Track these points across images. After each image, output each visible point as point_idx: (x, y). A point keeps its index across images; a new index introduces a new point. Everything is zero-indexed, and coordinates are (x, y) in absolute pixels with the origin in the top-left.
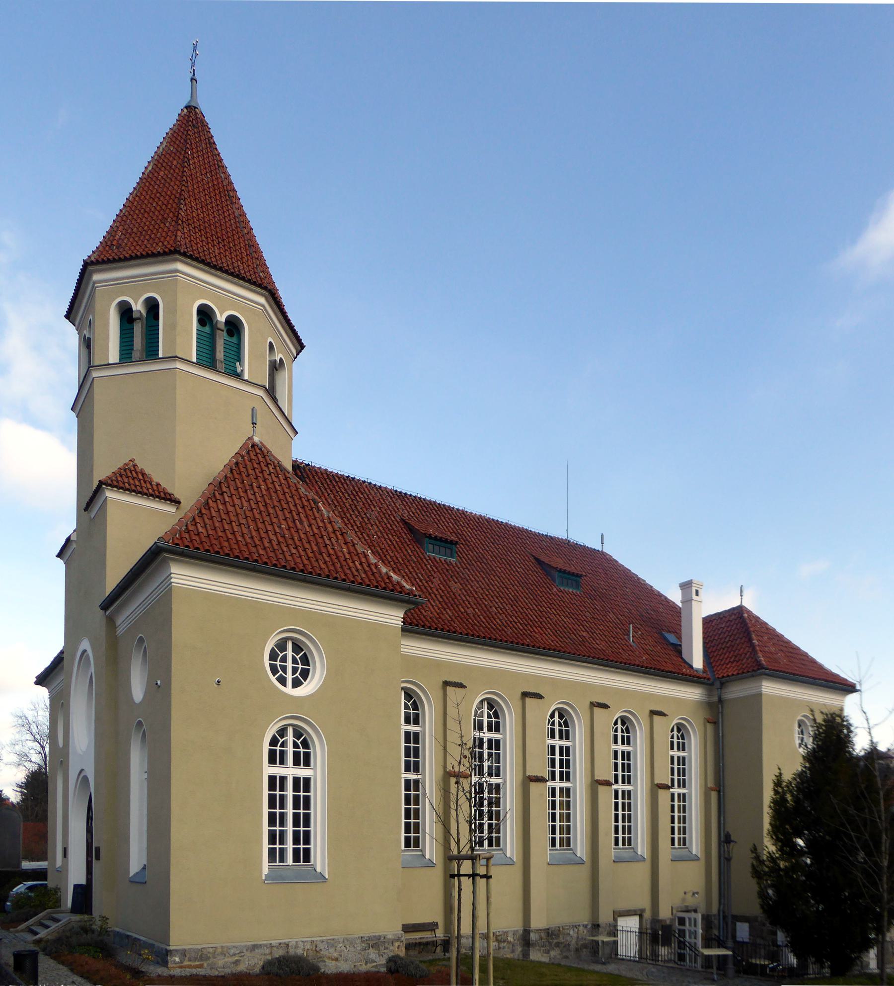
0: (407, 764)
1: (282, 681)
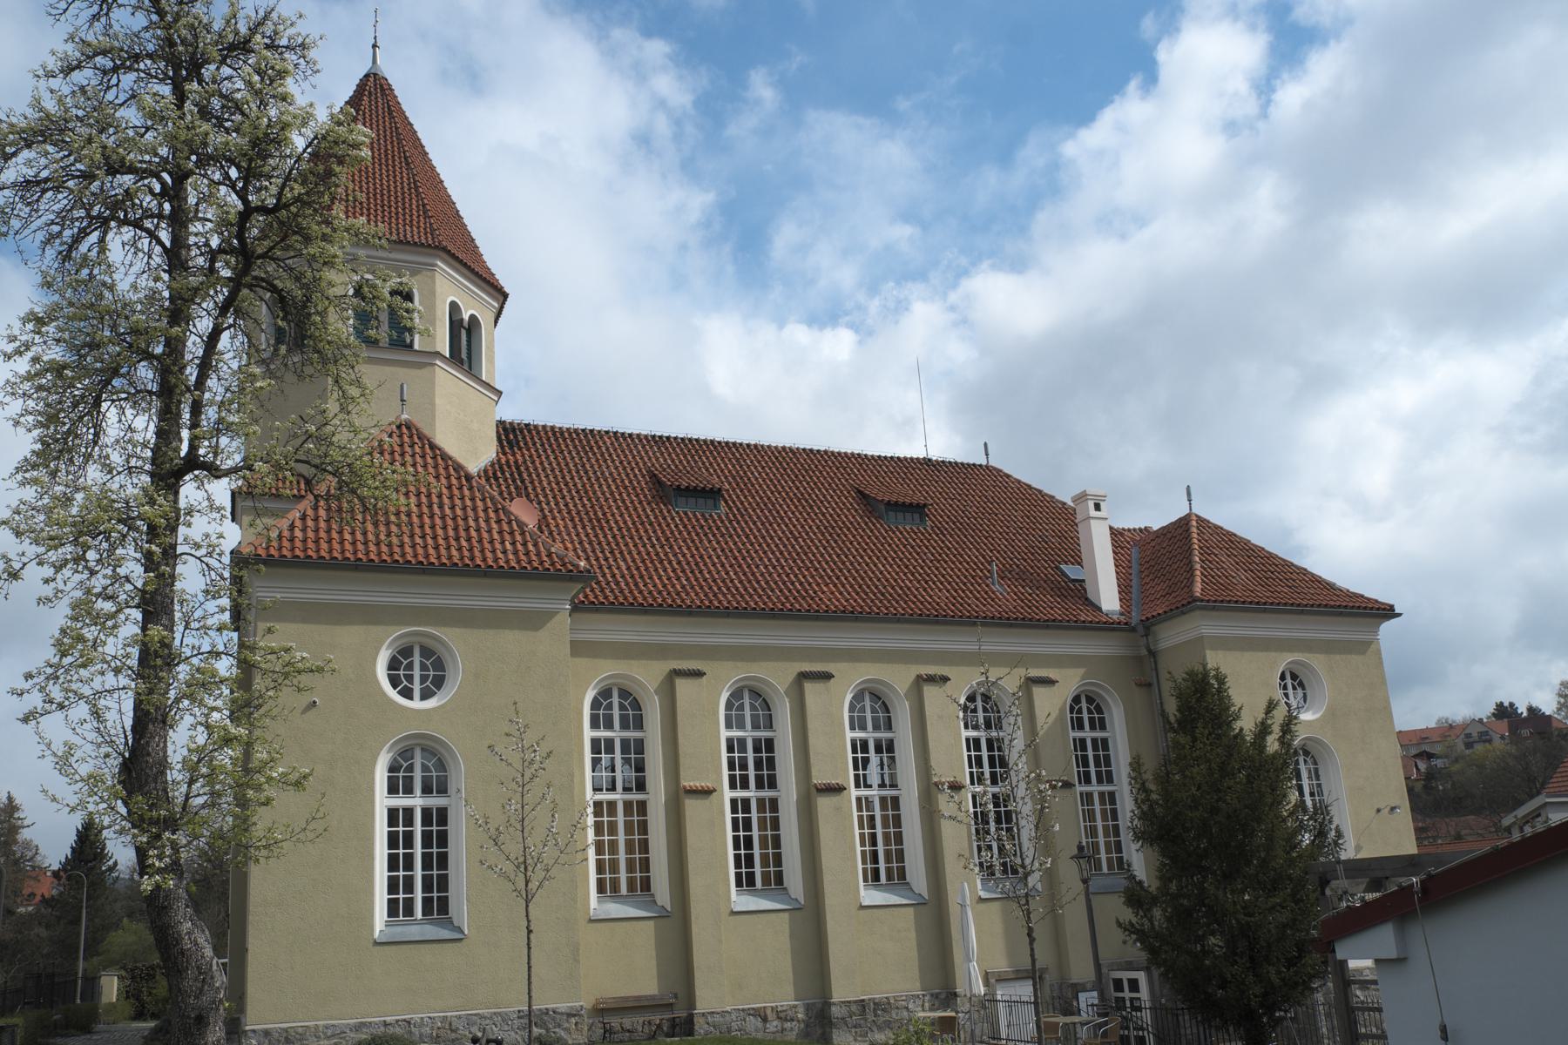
0: (732, 779)
1: (407, 693)
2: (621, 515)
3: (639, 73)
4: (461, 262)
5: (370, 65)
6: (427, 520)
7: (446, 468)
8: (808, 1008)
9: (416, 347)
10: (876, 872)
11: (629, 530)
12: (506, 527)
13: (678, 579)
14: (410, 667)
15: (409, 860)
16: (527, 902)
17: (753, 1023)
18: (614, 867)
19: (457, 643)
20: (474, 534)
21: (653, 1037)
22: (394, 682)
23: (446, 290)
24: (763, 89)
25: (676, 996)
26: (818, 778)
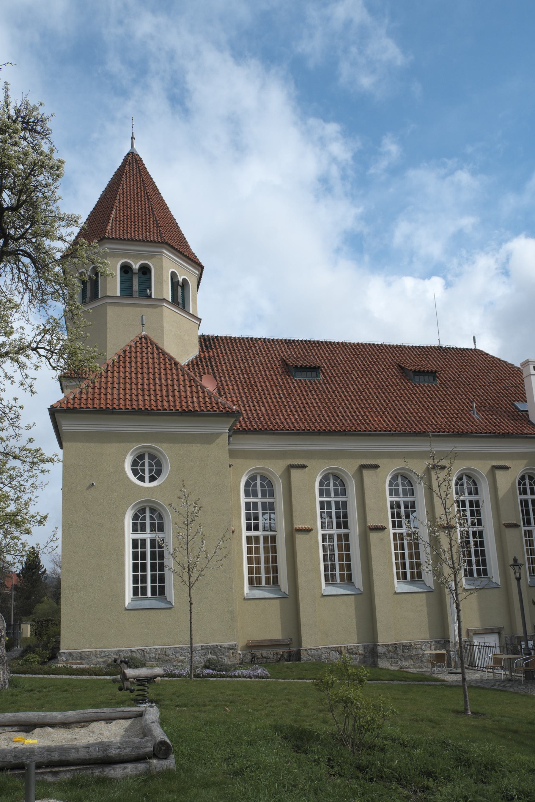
1: (142, 479)
2: (265, 382)
3: (323, 142)
4: (176, 250)
5: (130, 148)
6: (152, 387)
7: (164, 359)
8: (365, 647)
9: (153, 297)
10: (405, 574)
11: (268, 390)
12: (194, 389)
13: (293, 415)
14: (143, 465)
15: (144, 566)
16: (190, 588)
17: (334, 655)
18: (258, 571)
19: (168, 452)
20: (177, 393)
21: (278, 661)
22: (135, 472)
23: (167, 267)
24: (392, 148)
25: (291, 640)
26: (371, 523)
